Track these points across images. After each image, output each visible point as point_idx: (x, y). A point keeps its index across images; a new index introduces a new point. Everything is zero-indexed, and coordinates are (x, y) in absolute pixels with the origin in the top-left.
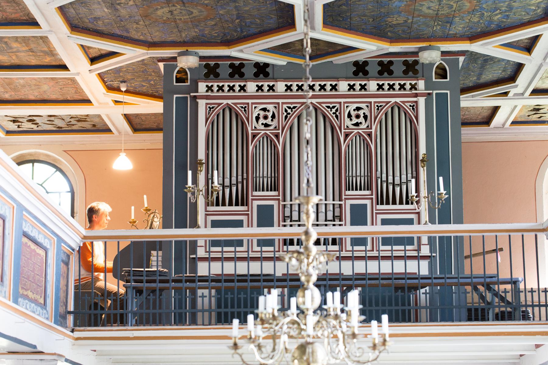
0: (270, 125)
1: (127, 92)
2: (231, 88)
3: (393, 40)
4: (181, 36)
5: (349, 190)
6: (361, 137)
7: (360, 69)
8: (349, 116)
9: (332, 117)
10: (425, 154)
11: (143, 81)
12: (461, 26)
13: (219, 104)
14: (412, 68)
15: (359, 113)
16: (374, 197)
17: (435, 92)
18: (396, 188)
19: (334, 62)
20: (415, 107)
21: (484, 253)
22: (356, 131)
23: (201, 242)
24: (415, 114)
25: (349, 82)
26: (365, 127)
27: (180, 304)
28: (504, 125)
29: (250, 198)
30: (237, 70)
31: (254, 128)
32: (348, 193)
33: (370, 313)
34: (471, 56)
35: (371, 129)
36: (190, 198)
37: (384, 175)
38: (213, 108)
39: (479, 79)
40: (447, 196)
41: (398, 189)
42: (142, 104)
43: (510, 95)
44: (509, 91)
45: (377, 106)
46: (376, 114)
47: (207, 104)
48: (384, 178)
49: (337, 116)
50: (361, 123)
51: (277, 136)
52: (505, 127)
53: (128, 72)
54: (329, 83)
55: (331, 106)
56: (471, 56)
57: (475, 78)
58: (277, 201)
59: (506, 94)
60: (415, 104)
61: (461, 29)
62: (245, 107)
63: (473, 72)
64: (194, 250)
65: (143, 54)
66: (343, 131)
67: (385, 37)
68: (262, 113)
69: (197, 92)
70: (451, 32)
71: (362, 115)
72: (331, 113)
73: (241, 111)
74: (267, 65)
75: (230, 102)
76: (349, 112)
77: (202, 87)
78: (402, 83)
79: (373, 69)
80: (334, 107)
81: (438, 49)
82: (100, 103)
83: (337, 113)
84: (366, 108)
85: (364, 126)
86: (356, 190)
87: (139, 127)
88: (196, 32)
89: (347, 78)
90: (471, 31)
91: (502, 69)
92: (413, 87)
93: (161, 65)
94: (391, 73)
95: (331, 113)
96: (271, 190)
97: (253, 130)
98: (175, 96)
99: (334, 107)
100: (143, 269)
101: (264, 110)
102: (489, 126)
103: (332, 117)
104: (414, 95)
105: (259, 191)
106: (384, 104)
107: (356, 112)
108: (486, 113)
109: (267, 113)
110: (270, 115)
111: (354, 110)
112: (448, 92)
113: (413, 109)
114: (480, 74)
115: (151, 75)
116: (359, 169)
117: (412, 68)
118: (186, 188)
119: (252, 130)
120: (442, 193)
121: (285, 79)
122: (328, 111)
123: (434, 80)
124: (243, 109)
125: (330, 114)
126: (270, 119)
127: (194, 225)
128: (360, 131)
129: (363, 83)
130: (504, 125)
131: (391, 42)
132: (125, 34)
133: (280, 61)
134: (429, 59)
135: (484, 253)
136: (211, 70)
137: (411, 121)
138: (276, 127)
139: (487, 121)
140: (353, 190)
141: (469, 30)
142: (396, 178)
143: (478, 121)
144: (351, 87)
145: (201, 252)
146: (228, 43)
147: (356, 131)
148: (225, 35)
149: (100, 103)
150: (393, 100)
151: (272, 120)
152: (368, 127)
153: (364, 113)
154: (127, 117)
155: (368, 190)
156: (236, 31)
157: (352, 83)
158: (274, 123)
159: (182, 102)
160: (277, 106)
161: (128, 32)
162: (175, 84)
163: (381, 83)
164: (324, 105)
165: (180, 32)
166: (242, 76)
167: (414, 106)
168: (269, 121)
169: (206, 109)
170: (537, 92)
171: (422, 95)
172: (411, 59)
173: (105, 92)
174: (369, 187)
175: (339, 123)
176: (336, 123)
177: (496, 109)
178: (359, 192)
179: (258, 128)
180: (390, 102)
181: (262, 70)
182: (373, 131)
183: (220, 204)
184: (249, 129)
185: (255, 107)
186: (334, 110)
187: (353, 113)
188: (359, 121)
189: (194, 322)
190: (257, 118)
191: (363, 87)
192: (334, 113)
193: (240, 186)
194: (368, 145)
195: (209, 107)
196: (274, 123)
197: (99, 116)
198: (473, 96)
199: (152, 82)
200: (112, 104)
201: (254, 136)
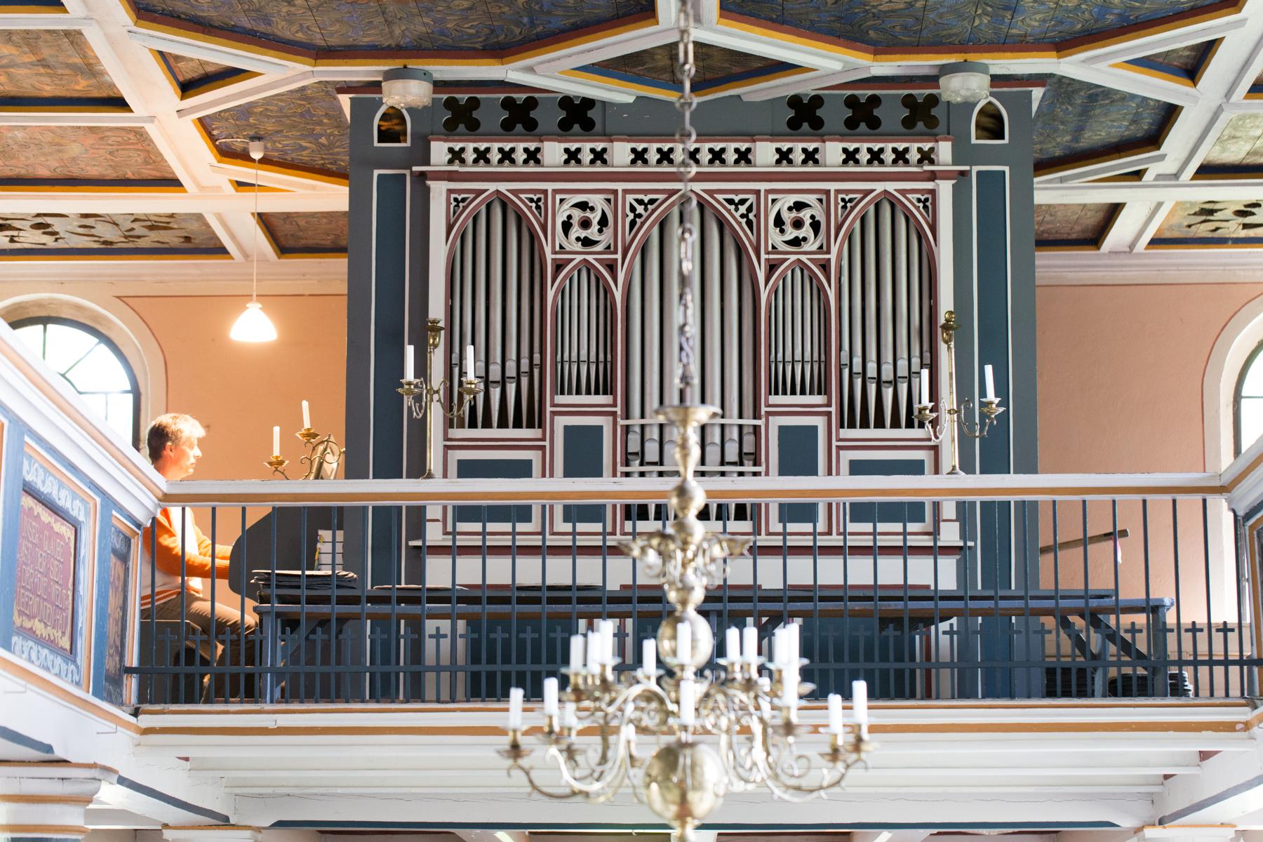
0: (595, 243)
1: (266, 161)
2: (507, 156)
3: (882, 48)
4: (391, 33)
5: (776, 393)
6: (806, 272)
7: (805, 114)
8: (779, 222)
9: (739, 224)
10: (951, 313)
11: (303, 137)
12: (1038, 17)
13: (479, 193)
14: (923, 113)
15: (801, 215)
16: (833, 409)
17: (975, 169)
18: (884, 389)
19: (745, 99)
20: (929, 202)
21: (1085, 541)
22: (793, 258)
23: (434, 511)
24: (930, 220)
25: (778, 145)
26: (815, 247)
27: (385, 652)
28: (1132, 246)
29: (549, 409)
30: (521, 113)
31: (557, 248)
32: (774, 399)
33: (825, 677)
34: (1060, 87)
35: (828, 252)
36: (410, 408)
37: (857, 361)
38: (463, 200)
39: (1076, 139)
40: (1001, 409)
41: (888, 393)
42: (301, 191)
43: (1148, 177)
44: (1145, 170)
45: (843, 200)
46: (840, 219)
47: (450, 191)
48: (857, 367)
49: (749, 223)
50: (805, 239)
51: (612, 267)
52: (1135, 251)
53: (269, 117)
54: (733, 146)
55: (737, 199)
56: (1060, 87)
57: (1068, 138)
58: (611, 418)
59: (1138, 175)
60: (930, 196)
61: (1036, 24)
62: (539, 200)
63: (1063, 123)
64: (418, 529)
65: (304, 75)
66: (763, 256)
67: (863, 42)
68: (577, 214)
69: (428, 164)
70: (1014, 31)
71: (808, 221)
72: (737, 215)
73: (530, 208)
74: (588, 103)
75: (503, 187)
76: (778, 214)
77: (439, 152)
78: (901, 146)
79: (834, 115)
80: (743, 202)
81: (983, 69)
82: (201, 188)
83: (751, 216)
84: (817, 204)
85: (811, 245)
86: (793, 392)
87: (291, 243)
88: (424, 24)
89: (774, 136)
90: (1060, 28)
91: (1130, 117)
92: (926, 157)
93: (345, 100)
94: (874, 123)
95: (737, 215)
96: (597, 393)
97: (556, 253)
98: (376, 172)
99: (743, 202)
100: (299, 573)
101: (583, 206)
102: (1099, 249)
103: (739, 224)
104: (928, 175)
105: (570, 393)
106: (859, 196)
107: (794, 214)
108: (1092, 220)
109: (588, 214)
110: (595, 217)
111: (790, 209)
112: (1006, 169)
113: (925, 207)
114: (1080, 130)
115: (320, 123)
116: (799, 346)
117: (923, 113)
118: (402, 386)
119: (554, 252)
120: (992, 403)
121: (631, 136)
122: (729, 211)
123: (974, 141)
124: (534, 205)
125: (734, 217)
126: (595, 227)
127: (419, 470)
128: (804, 258)
129: (811, 147)
130: (1132, 246)
131: (876, 53)
132: (262, 28)
133: (619, 93)
134: (963, 92)
135: (1085, 541)
136: (459, 112)
137: (921, 236)
138: (609, 247)
139: (1094, 237)
140: (785, 393)
141: (1054, 26)
142: (884, 367)
143: (1074, 236)
144: (784, 156)
145: (434, 535)
146: (500, 50)
147: (793, 258)
148: (493, 31)
149: (201, 188)
150: (879, 187)
151: (600, 231)
152: (821, 247)
153: (812, 217)
154: (265, 220)
155: (820, 393)
156: (518, 24)
157: (785, 146)
158: (605, 238)
159: (392, 187)
160: (611, 197)
161: (269, 23)
162: (376, 144)
163: (852, 147)
164: (720, 197)
165: (389, 23)
166: (531, 127)
167: (927, 200)
168: (592, 232)
169: (448, 204)
170: (1208, 171)
171: (946, 175)
172: (921, 93)
173: (214, 162)
174: (822, 387)
175: (753, 239)
176: (747, 237)
177: (1114, 210)
178: (798, 399)
179: (568, 247)
180: (873, 191)
181: (578, 115)
182: (833, 257)
183: (480, 424)
184: (548, 250)
185: (562, 200)
186: (743, 209)
187: (788, 217)
188: (801, 233)
189: (416, 693)
190: (567, 226)
191: (810, 157)
192: (742, 216)
193: (525, 381)
194: (821, 291)
195: (456, 200)
196: (605, 238)
197: (199, 217)
198: (1062, 180)
199: (323, 140)
200: (230, 189)
201: (559, 267)
